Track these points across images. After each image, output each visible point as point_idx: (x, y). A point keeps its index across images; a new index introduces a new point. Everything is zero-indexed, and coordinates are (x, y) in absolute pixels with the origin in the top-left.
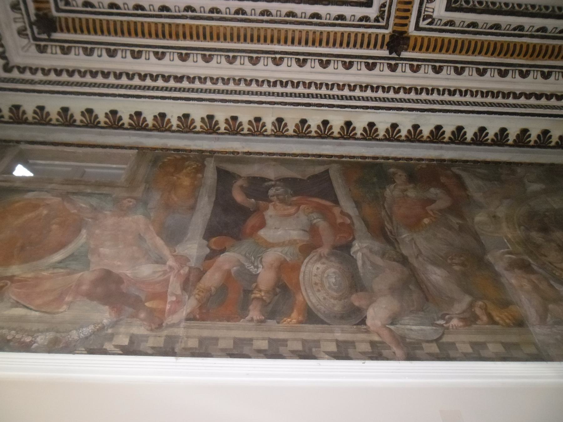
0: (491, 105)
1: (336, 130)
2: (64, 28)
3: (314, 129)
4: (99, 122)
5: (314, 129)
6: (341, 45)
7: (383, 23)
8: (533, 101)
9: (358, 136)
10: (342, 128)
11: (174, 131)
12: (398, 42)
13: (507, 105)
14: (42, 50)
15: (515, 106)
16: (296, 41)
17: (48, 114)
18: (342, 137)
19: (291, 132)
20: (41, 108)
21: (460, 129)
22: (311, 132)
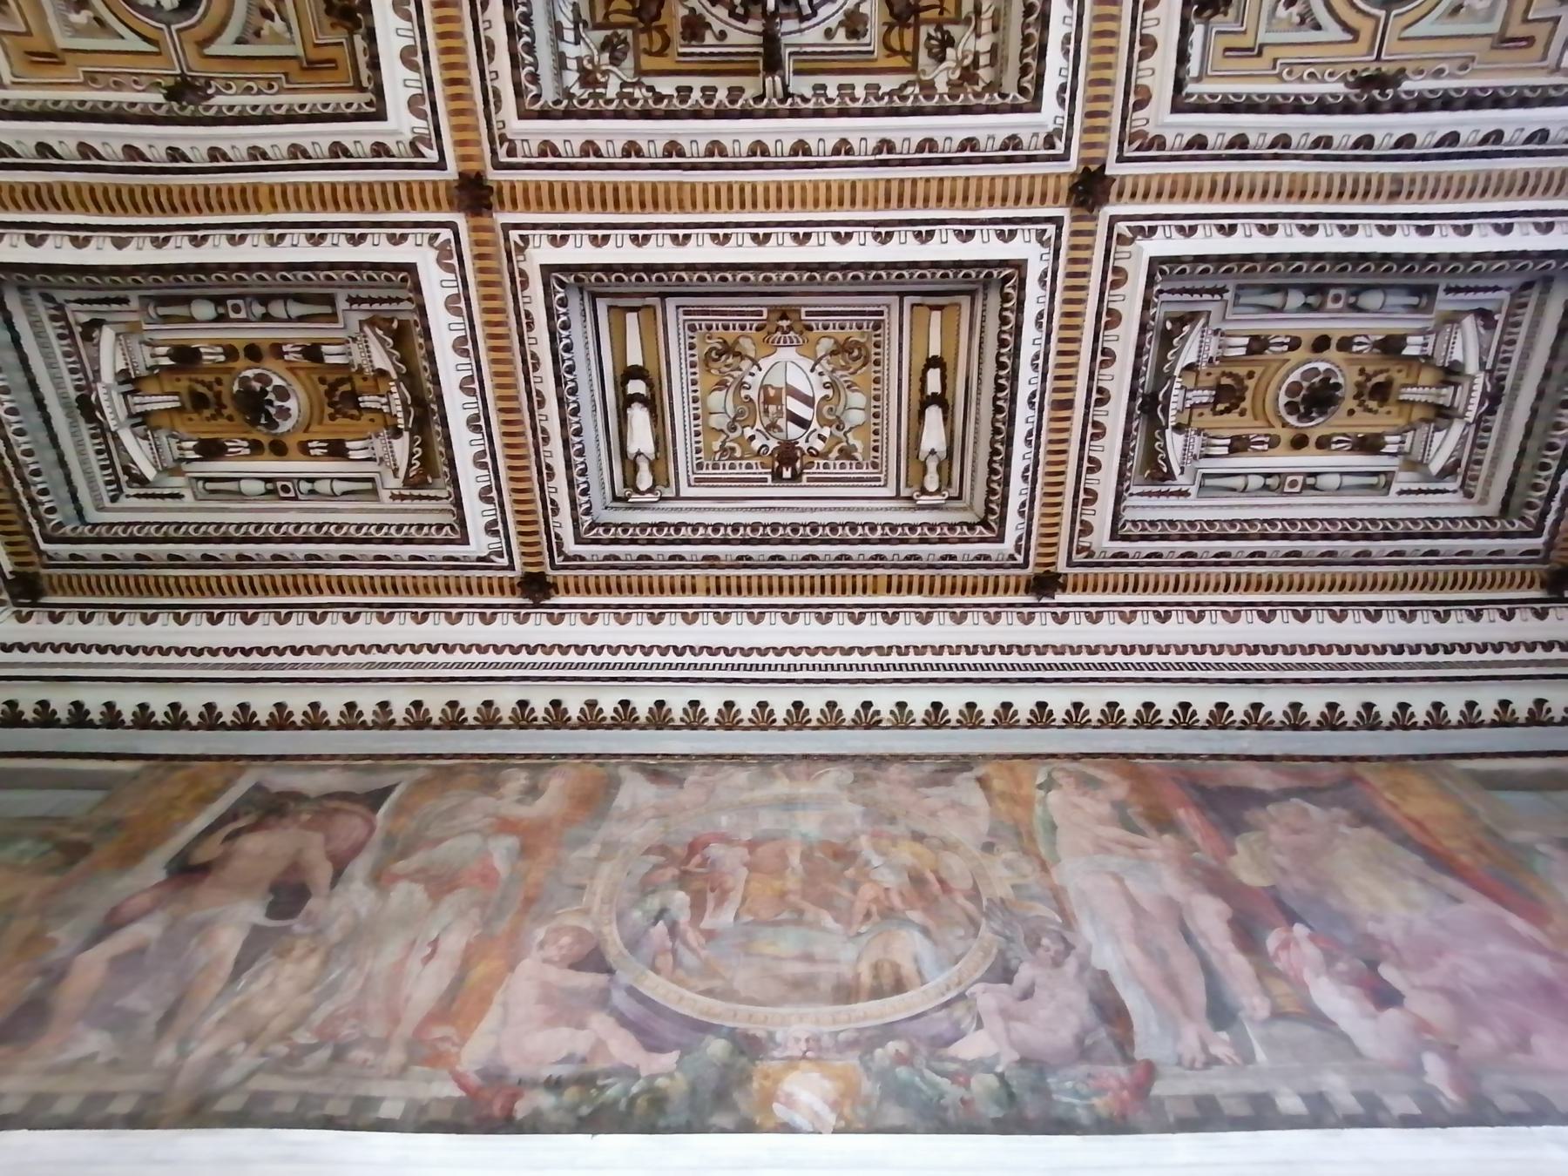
0: (1302, 666)
1: (954, 716)
2: (153, 589)
3: (540, 713)
4: (672, 720)
5: (540, 713)
6: (931, 591)
7: (558, 561)
8: (1317, 658)
9: (471, 721)
10: (514, 710)
11: (333, 728)
12: (1045, 584)
13: (1026, 667)
14: (22, 619)
15: (1038, 667)
16: (1110, 586)
17: (291, 714)
18: (928, 725)
19: (919, 723)
20: (453, 704)
21: (143, 707)
22: (535, 719)
